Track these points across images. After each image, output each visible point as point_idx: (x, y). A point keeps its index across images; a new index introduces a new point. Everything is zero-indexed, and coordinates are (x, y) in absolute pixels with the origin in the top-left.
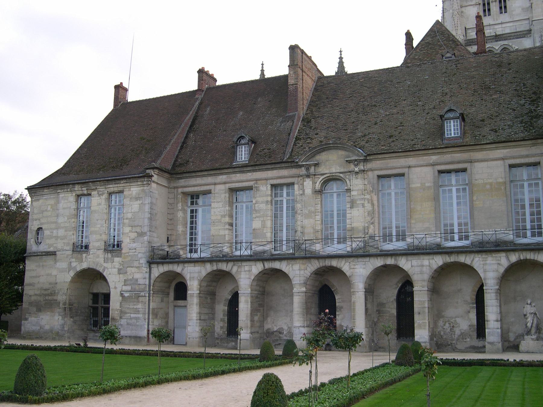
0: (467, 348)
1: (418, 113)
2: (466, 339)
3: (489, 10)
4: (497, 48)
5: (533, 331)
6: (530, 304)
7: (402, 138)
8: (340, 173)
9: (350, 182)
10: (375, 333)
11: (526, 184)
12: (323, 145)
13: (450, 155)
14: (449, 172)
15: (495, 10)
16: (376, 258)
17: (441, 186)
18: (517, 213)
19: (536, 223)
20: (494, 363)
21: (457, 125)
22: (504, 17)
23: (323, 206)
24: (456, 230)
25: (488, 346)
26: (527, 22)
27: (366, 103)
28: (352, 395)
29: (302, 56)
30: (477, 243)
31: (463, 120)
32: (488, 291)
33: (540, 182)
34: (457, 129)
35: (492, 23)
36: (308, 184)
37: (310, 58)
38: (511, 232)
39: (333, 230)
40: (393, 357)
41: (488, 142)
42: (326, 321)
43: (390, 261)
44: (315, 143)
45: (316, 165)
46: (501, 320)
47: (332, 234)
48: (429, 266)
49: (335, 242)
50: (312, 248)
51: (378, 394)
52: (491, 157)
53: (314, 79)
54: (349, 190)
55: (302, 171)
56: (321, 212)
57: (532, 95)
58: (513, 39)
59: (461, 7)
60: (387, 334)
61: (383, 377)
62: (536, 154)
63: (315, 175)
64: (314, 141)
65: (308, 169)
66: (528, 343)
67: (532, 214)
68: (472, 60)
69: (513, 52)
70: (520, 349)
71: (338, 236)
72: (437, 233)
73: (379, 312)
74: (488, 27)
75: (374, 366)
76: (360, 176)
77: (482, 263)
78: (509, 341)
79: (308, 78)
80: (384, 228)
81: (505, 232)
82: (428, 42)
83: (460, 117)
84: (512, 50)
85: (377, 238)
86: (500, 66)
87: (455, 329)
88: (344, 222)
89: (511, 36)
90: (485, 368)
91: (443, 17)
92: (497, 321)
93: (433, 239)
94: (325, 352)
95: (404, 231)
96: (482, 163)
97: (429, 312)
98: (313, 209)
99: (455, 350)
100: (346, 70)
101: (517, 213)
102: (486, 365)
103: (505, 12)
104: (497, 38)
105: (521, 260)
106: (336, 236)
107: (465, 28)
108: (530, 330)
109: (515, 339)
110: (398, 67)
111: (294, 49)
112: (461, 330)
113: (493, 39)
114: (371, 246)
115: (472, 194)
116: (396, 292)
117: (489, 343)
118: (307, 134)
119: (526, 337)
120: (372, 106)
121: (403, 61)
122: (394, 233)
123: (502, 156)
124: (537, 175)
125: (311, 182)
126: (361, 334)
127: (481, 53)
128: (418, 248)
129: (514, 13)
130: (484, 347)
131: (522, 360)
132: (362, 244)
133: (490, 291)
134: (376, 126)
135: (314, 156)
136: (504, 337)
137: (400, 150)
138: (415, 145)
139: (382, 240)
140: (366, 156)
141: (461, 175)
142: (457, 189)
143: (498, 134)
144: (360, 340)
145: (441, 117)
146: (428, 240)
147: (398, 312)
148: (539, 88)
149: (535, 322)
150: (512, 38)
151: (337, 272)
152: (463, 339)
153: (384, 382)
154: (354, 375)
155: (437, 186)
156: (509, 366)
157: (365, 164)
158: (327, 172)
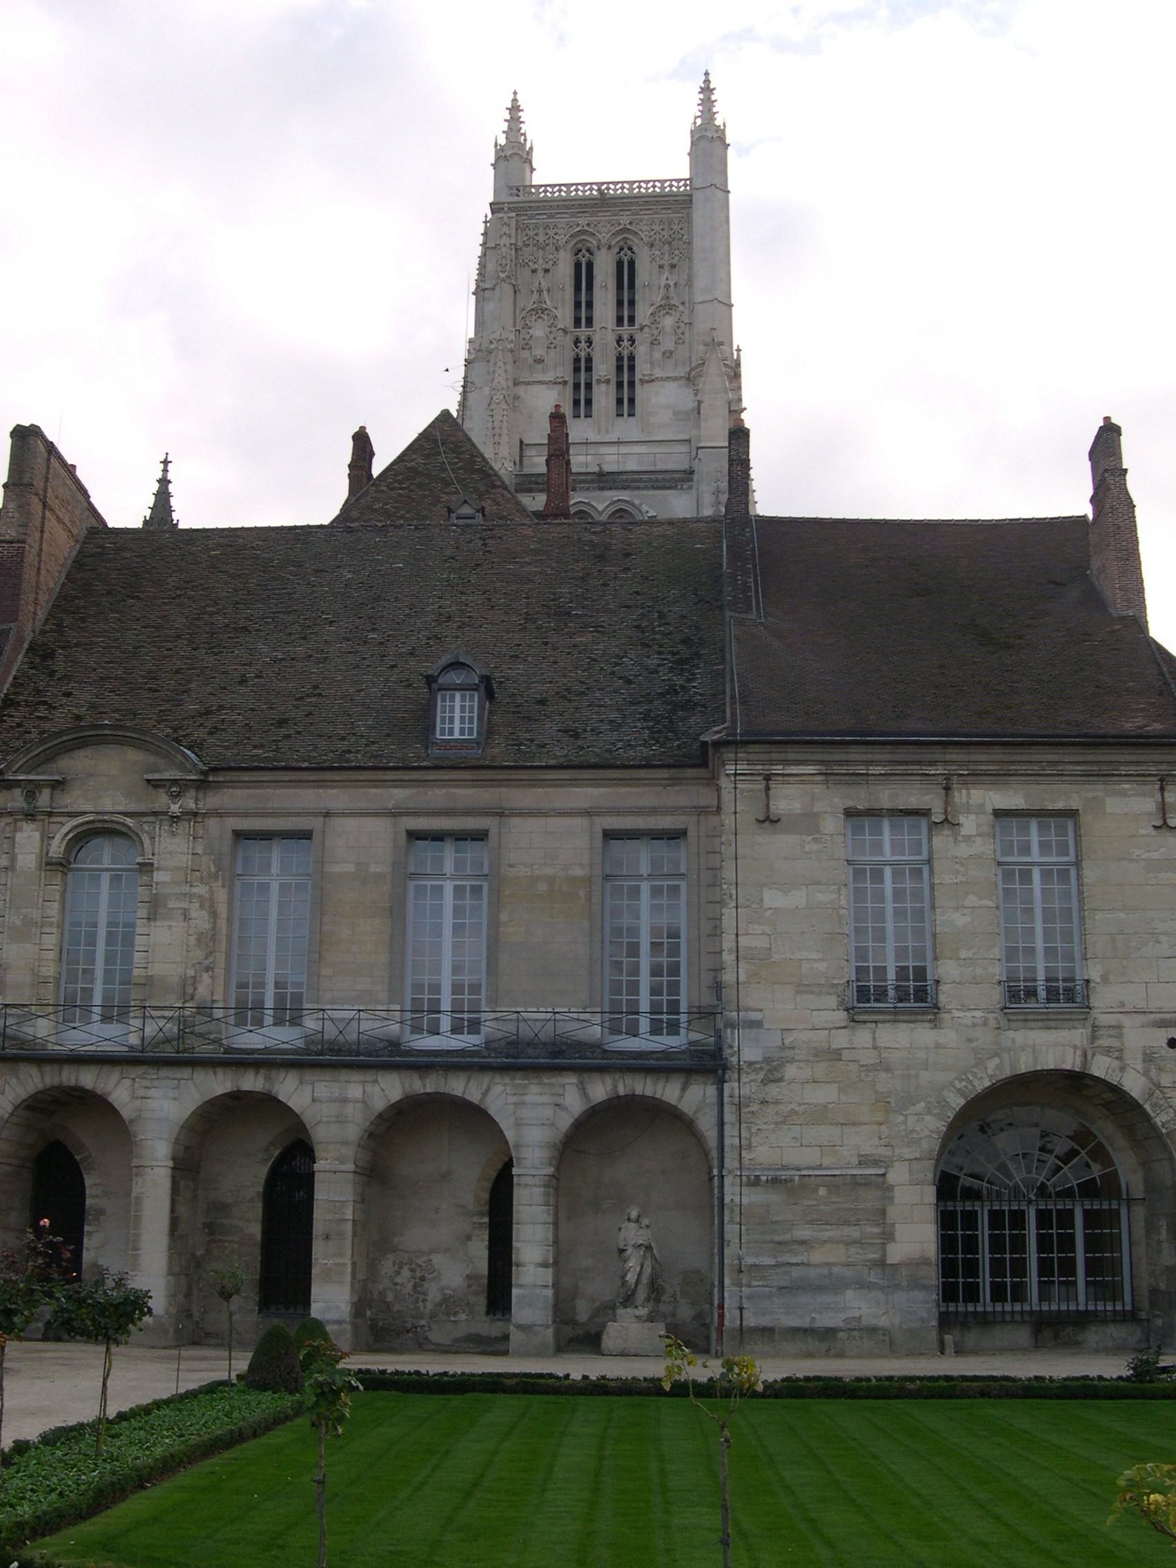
0: (455, 1340)
1: (366, 663)
2: (455, 1314)
3: (589, 402)
4: (600, 507)
5: (641, 1294)
6: (637, 1221)
7: (312, 728)
8: (126, 814)
9: (153, 844)
10: (195, 1291)
11: (645, 887)
12: (82, 729)
13: (444, 791)
14: (438, 837)
15: (603, 404)
16: (211, 1072)
17: (413, 876)
18: (617, 966)
19: (665, 998)
20: (529, 1385)
21: (471, 707)
22: (626, 428)
23: (68, 907)
24: (446, 1005)
25: (516, 1337)
26: (684, 448)
27: (220, 620)
28: (108, 1478)
29: (48, 460)
30: (503, 1043)
31: (490, 695)
32: (524, 1180)
33: (683, 885)
34: (471, 719)
35: (593, 437)
36: (28, 838)
37: (71, 470)
38: (597, 1019)
39: (92, 981)
40: (242, 1363)
41: (552, 762)
42: (40, 1254)
43: (251, 1082)
44: (60, 719)
45: (58, 785)
46: (556, 1263)
47: (88, 993)
48: (364, 1102)
49: (96, 1018)
50: (25, 1029)
51: (185, 1477)
52: (558, 805)
53: (75, 532)
54: (147, 868)
55: (13, 800)
56: (60, 926)
57: (680, 647)
58: (645, 488)
59: (515, 384)
60: (226, 1295)
61: (209, 1422)
62: (678, 808)
63: (50, 814)
64: (57, 713)
65: (31, 795)
66: (628, 1328)
67: (656, 971)
68: (529, 532)
69: (641, 523)
70: (603, 1345)
71: (105, 997)
72: (393, 1007)
73: (211, 1228)
74: (583, 449)
75: (182, 1391)
76: (183, 827)
77: (511, 1099)
78: (574, 1323)
79: (59, 527)
80: (242, 985)
81: (582, 1016)
82: (412, 469)
83: (482, 688)
84: (639, 518)
85: (218, 1014)
86: (601, 558)
87: (426, 1285)
88: (127, 957)
89: (640, 480)
90: (501, 1399)
91: (463, 404)
92: (545, 1265)
93: (378, 1024)
94: (41, 1345)
95: (298, 998)
96: (531, 820)
97: (354, 1235)
98: (35, 914)
99: (423, 1346)
100: (175, 516)
101: (617, 966)
102: (506, 1390)
103: (631, 415)
104: (604, 480)
105: (619, 1097)
106: (98, 999)
107: (521, 442)
108: (634, 1291)
109: (592, 1317)
110: (321, 527)
111: (27, 439)
112: (442, 1289)
113: (592, 481)
114: (201, 1035)
115: (496, 903)
116: (264, 1172)
117: (519, 1327)
118: (38, 692)
119: (620, 1311)
120: (235, 629)
121: (337, 512)
122: (269, 1002)
123: (585, 805)
124: (677, 864)
125: (37, 835)
126: (147, 1295)
127: (556, 516)
128: (334, 1048)
129: (652, 420)
130: (506, 1337)
131: (603, 1377)
132: (172, 1028)
133: (529, 1180)
134: (243, 690)
135: (51, 757)
136: (562, 1310)
137: (306, 765)
138: (349, 752)
139: (232, 1020)
140: (205, 773)
141: (472, 851)
142: (455, 887)
143: (580, 743)
144: (143, 1314)
145: (430, 680)
146: (365, 1026)
147: (265, 1233)
148: (698, 628)
149: (648, 1270)
150: (642, 485)
151: (95, 1105)
152: (448, 1314)
153: (206, 1437)
154: (122, 1417)
155: (403, 875)
156: (567, 1393)
157: (201, 795)
158: (89, 808)
